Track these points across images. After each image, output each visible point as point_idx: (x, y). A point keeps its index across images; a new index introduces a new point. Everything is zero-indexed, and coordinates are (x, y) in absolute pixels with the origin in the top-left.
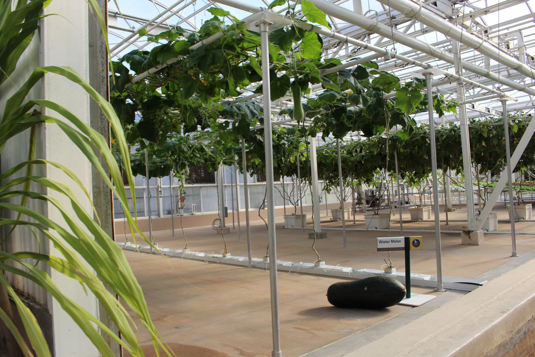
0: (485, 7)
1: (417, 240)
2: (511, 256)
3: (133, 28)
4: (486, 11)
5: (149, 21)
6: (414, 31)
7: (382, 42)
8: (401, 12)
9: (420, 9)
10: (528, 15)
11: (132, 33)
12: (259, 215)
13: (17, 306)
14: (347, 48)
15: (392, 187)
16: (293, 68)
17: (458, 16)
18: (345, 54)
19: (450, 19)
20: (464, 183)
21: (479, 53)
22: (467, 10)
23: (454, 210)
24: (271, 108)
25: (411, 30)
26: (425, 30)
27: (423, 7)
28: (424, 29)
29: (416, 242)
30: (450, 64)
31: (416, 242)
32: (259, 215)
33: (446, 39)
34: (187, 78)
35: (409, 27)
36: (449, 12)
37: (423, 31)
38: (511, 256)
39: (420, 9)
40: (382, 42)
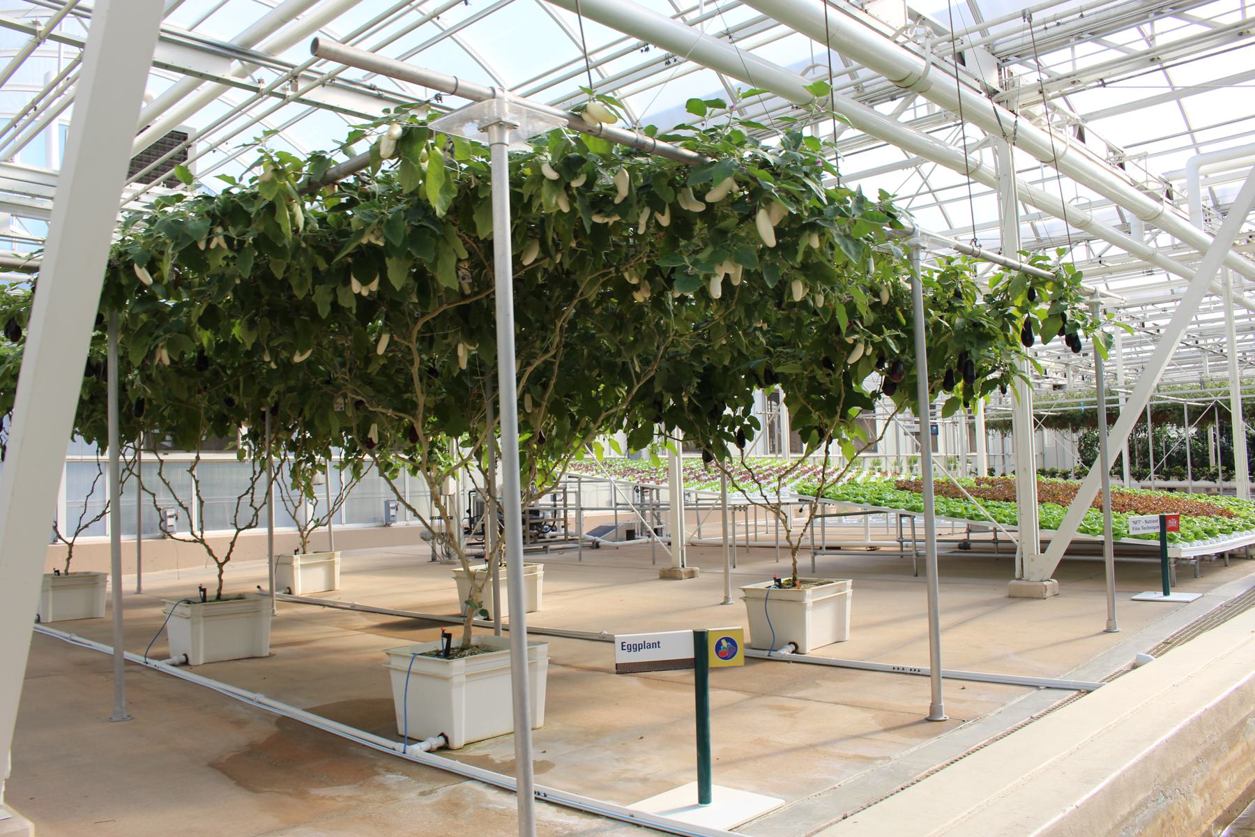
1: (728, 639)
2: (437, 654)
3: (260, 81)
5: (293, 67)
9: (927, 70)
10: (1092, 119)
11: (254, 93)
12: (239, 498)
16: (368, 225)
23: (692, 575)
25: (907, 116)
27: (933, 64)
29: (724, 643)
31: (724, 643)
32: (239, 498)
33: (906, 158)
35: (904, 108)
36: (993, 81)
38: (437, 654)
39: (927, 70)
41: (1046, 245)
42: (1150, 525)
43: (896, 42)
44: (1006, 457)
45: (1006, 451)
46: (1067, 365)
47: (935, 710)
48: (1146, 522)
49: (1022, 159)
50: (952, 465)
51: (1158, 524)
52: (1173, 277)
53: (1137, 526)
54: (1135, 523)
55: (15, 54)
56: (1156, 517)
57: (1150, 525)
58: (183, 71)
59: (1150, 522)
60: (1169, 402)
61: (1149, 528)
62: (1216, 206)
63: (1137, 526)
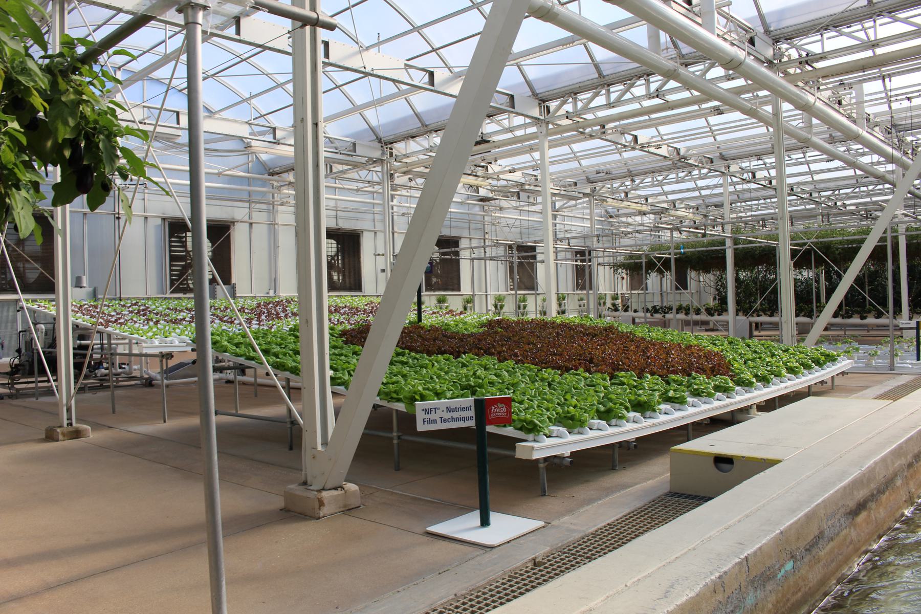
0: (821, 52)
4: (873, 46)
6: (523, 123)
7: (622, 99)
8: (694, 48)
13: (801, 390)
14: (648, 83)
15: (604, 257)
17: (780, 61)
18: (645, 94)
19: (770, 64)
20: (294, 314)
21: (792, 107)
22: (794, 54)
24: (326, 209)
26: (732, 77)
28: (650, 95)
30: (755, 120)
34: (113, 169)
37: (728, 77)
40: (622, 99)
41: (609, 81)
42: (456, 415)
43: (725, 40)
44: (664, 295)
45: (664, 289)
46: (705, 216)
47: (892, 367)
48: (449, 410)
49: (786, 106)
50: (602, 301)
51: (472, 413)
52: (859, 172)
53: (432, 416)
54: (427, 411)
55: (123, 23)
56: (470, 401)
57: (456, 415)
58: (445, 94)
59: (456, 409)
60: (763, 245)
61: (453, 419)
62: (767, 31)
63: (432, 416)
